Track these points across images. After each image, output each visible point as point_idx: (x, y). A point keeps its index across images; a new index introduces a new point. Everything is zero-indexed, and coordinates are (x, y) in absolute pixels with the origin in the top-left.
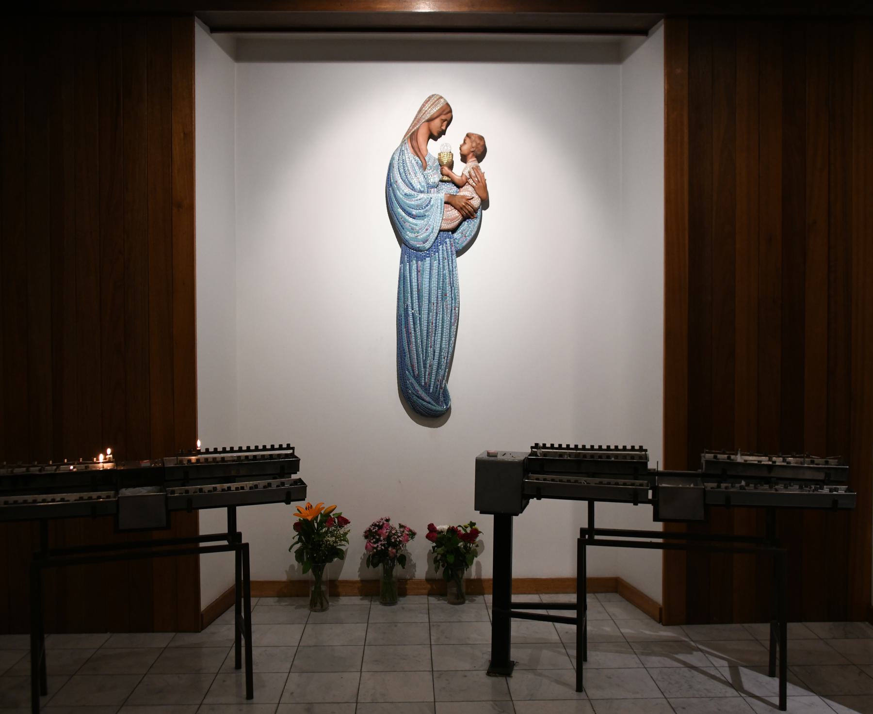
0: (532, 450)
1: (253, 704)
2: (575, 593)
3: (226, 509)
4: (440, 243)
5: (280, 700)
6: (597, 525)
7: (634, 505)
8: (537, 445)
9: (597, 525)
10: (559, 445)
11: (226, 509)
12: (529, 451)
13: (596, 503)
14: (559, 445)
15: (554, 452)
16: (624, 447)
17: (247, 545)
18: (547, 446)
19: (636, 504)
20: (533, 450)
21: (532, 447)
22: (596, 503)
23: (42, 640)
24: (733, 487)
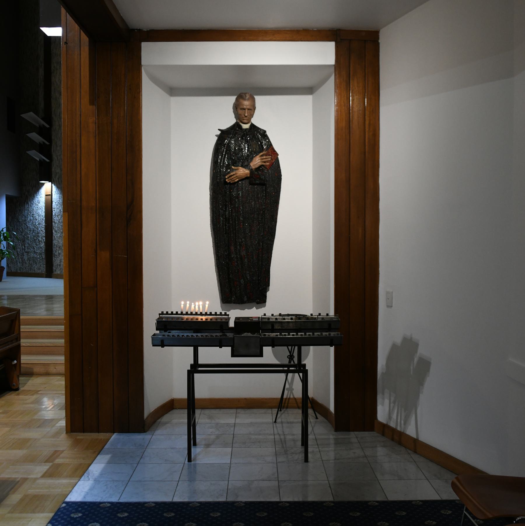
0: (159, 316)
1: (195, 481)
2: (64, 410)
3: (193, 348)
4: (14, 248)
5: (228, 482)
6: (200, 362)
7: (220, 348)
8: (162, 312)
9: (200, 362)
10: (171, 312)
11: (193, 348)
12: (158, 316)
13: (302, 347)
14: (171, 312)
15: (9, 315)
16: (176, 312)
17: (307, 370)
18: (178, 313)
19: (221, 347)
20: (161, 316)
21: (160, 314)
22: (302, 347)
23: (194, 412)
24: (289, 335)
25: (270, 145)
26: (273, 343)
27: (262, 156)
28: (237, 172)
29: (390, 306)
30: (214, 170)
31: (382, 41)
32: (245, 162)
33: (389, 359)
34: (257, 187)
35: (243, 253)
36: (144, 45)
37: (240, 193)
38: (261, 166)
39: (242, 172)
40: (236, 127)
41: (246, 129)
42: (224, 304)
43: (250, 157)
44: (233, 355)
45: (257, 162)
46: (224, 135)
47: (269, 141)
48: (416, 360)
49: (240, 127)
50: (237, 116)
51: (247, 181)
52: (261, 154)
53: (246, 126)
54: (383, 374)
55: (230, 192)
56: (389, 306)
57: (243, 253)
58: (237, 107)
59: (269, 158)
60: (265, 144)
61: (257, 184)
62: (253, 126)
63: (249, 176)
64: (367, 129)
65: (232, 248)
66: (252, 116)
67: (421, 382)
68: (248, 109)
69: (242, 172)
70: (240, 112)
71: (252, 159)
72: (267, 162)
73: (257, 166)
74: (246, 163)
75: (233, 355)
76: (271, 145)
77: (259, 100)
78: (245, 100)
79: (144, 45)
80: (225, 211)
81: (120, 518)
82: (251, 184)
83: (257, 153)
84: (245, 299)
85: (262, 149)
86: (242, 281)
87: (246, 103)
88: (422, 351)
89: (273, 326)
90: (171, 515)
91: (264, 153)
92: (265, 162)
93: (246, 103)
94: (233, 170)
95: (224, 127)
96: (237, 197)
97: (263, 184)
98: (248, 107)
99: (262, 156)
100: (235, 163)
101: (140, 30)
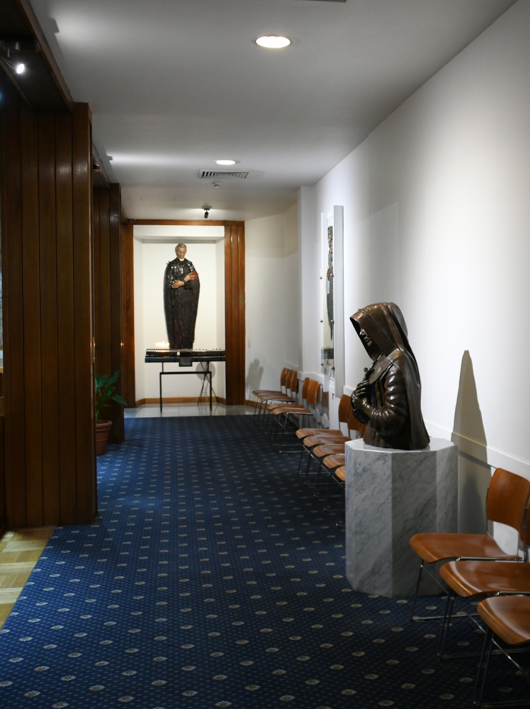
25: (194, 269)
26: (196, 360)
27: (190, 275)
28: (178, 283)
29: (249, 347)
30: (166, 282)
31: (246, 226)
32: (182, 277)
33: (250, 369)
34: (177, 267)
35: (181, 323)
36: (223, 348)
37: (179, 293)
38: (190, 280)
39: (180, 283)
40: (176, 262)
41: (182, 262)
42: (30, 573)
43: (184, 276)
44: (180, 366)
45: (188, 278)
46: (170, 264)
47: (194, 267)
48: (259, 368)
49: (179, 260)
50: (177, 255)
51: (183, 287)
52: (190, 274)
53: (182, 260)
54: (247, 378)
55: (174, 293)
56: (249, 347)
57: (181, 323)
58: (177, 250)
59: (194, 276)
60: (192, 269)
61: (188, 289)
62: (185, 260)
63: (184, 285)
64: (239, 266)
65: (175, 321)
66: (184, 255)
67: (260, 378)
68: (184, 252)
69: (180, 283)
70: (179, 253)
71: (185, 276)
72: (193, 278)
73: (188, 280)
74: (182, 279)
75: (180, 366)
76: (195, 269)
77: (188, 245)
78: (181, 247)
79: (223, 348)
80: (172, 302)
81: (13, 664)
82: (185, 289)
83: (188, 274)
84: (182, 347)
85: (190, 271)
86: (180, 338)
87: (182, 249)
88: (261, 364)
89: (196, 354)
90: (82, 635)
91: (191, 273)
92: (192, 278)
93: (182, 249)
94: (175, 282)
95: (171, 260)
96: (178, 295)
97: (191, 289)
98: (183, 251)
99: (190, 275)
100: (176, 278)
101: (133, 220)
